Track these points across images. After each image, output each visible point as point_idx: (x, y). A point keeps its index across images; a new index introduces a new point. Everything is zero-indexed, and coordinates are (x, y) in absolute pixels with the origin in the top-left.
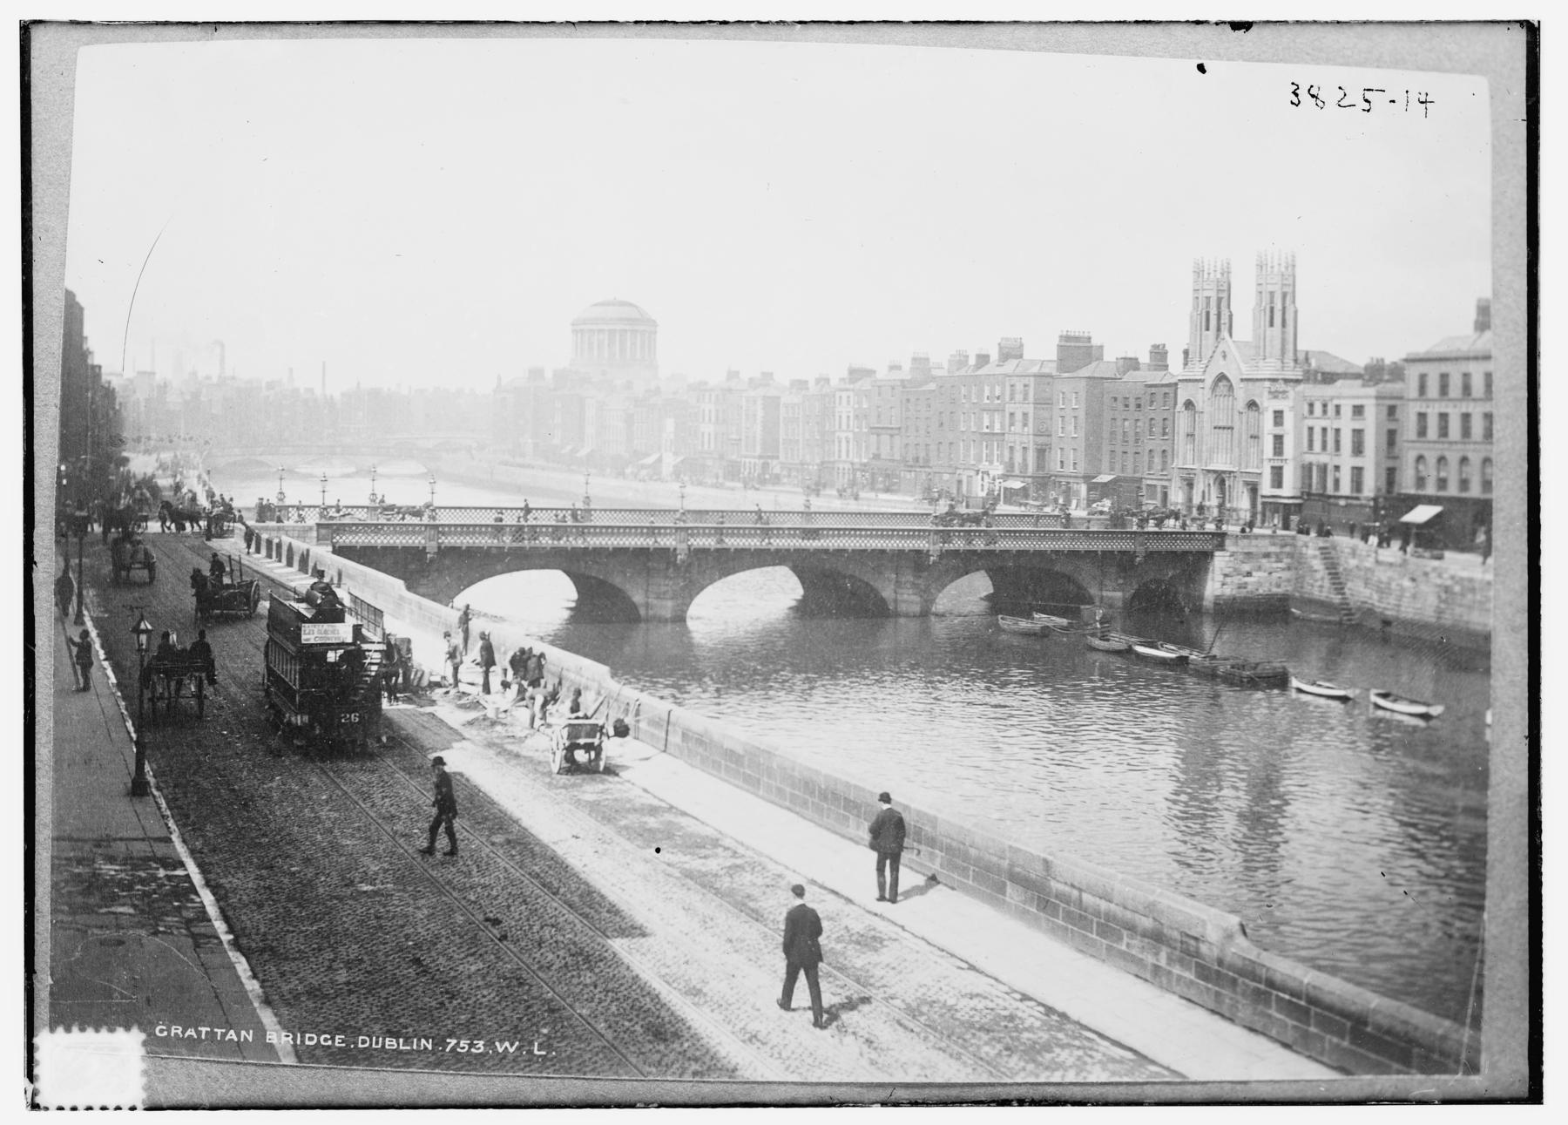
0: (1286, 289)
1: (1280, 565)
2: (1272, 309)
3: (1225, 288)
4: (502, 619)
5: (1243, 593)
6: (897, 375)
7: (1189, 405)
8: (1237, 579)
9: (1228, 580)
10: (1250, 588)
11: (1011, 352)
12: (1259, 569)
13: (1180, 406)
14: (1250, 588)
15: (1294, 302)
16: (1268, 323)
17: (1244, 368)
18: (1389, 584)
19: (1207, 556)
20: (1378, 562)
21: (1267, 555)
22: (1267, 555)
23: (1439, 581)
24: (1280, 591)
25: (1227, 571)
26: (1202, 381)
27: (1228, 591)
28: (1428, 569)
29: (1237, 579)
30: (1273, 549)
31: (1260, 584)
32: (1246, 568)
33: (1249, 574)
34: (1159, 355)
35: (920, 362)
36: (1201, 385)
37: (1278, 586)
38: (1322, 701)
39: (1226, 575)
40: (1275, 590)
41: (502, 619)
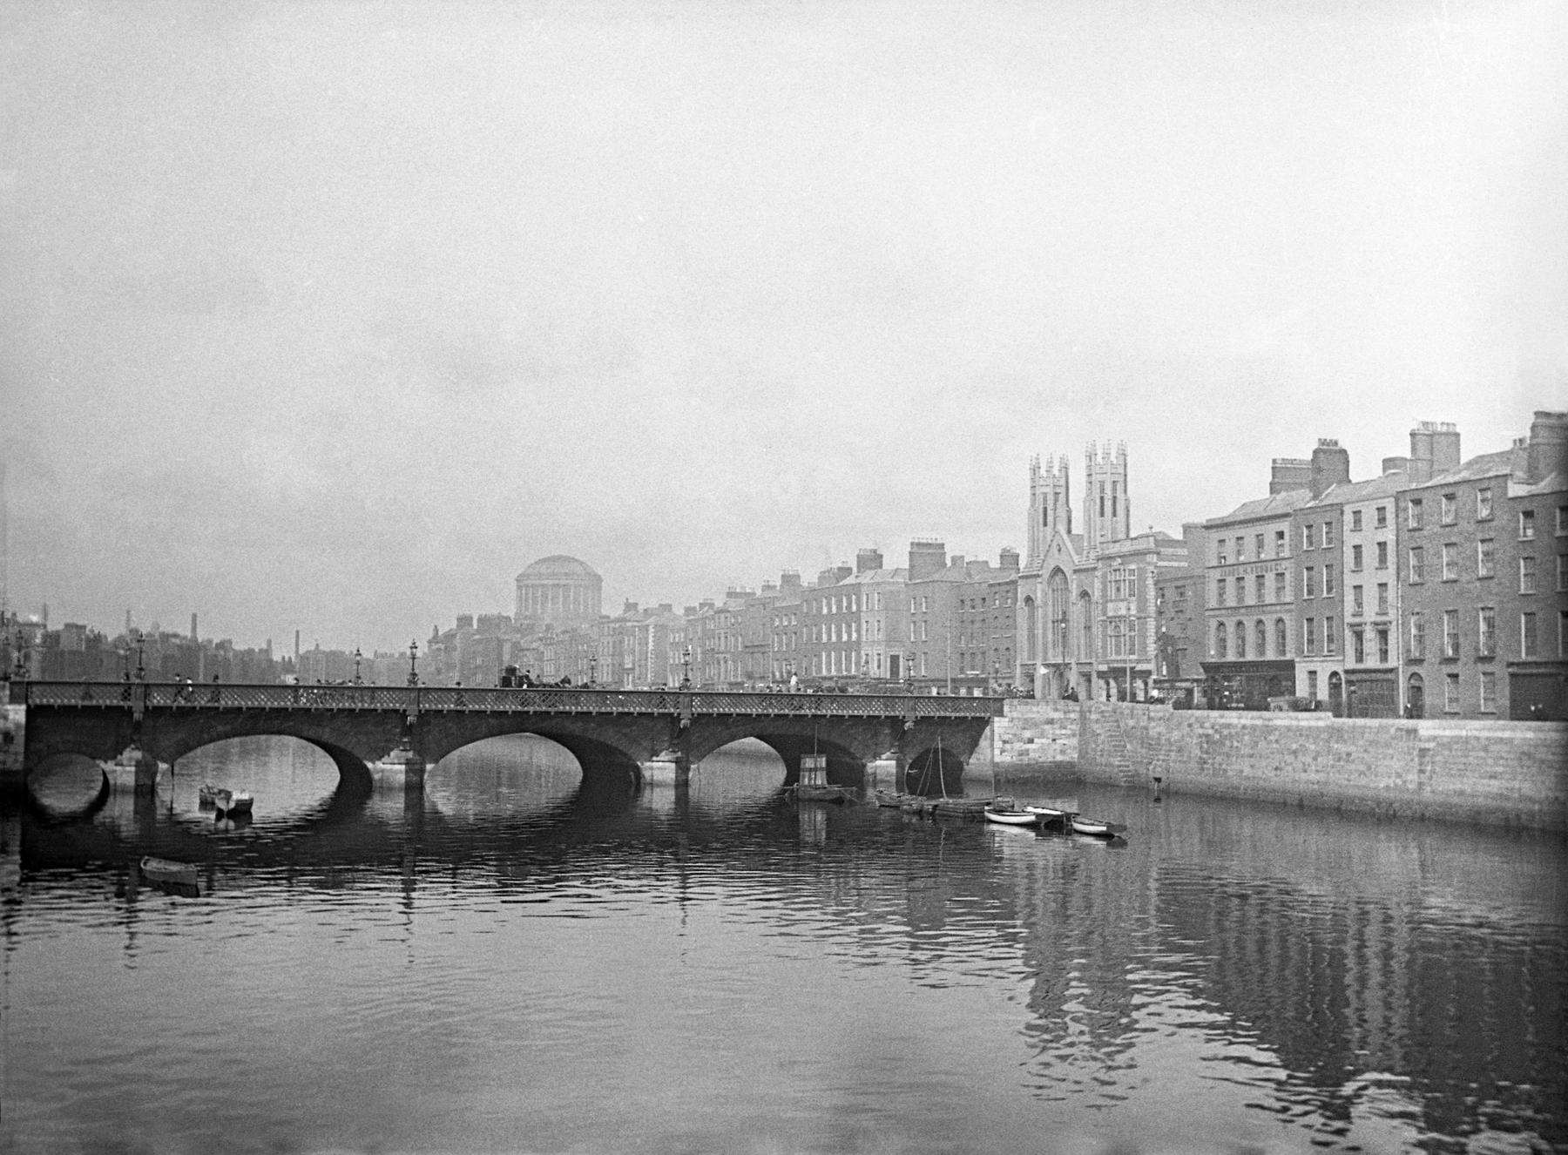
0: (1116, 478)
1: (1064, 732)
2: (1102, 499)
3: (1063, 482)
4: (400, 913)
5: (1025, 759)
6: (770, 594)
7: (1029, 600)
8: (1018, 746)
9: (1008, 746)
10: (1032, 755)
11: (872, 560)
12: (1042, 736)
13: (1020, 603)
14: (1032, 755)
15: (1125, 491)
16: (1098, 514)
17: (1076, 558)
18: (1159, 738)
19: (982, 723)
20: (1150, 718)
21: (1051, 722)
22: (1051, 722)
23: (1201, 731)
24: (1066, 758)
25: (1006, 737)
26: (1038, 576)
27: (1006, 758)
28: (1192, 720)
29: (1018, 746)
30: (1056, 715)
31: (1043, 749)
32: (1027, 734)
33: (1031, 741)
34: (1009, 558)
35: (790, 580)
36: (1039, 580)
37: (1063, 752)
38: (1016, 830)
39: (1005, 742)
40: (1059, 758)
41: (400, 913)
